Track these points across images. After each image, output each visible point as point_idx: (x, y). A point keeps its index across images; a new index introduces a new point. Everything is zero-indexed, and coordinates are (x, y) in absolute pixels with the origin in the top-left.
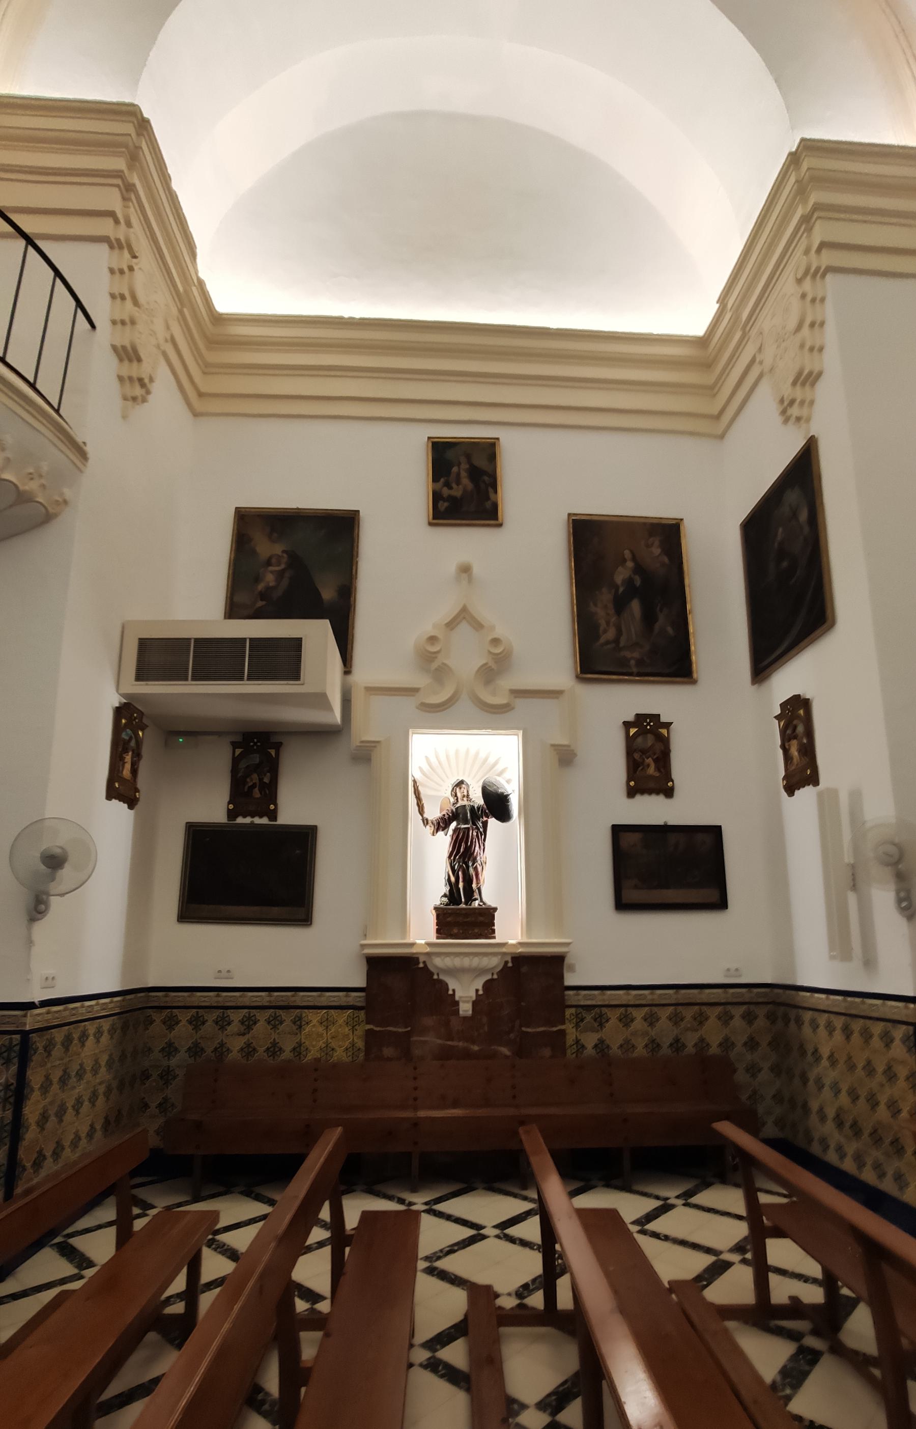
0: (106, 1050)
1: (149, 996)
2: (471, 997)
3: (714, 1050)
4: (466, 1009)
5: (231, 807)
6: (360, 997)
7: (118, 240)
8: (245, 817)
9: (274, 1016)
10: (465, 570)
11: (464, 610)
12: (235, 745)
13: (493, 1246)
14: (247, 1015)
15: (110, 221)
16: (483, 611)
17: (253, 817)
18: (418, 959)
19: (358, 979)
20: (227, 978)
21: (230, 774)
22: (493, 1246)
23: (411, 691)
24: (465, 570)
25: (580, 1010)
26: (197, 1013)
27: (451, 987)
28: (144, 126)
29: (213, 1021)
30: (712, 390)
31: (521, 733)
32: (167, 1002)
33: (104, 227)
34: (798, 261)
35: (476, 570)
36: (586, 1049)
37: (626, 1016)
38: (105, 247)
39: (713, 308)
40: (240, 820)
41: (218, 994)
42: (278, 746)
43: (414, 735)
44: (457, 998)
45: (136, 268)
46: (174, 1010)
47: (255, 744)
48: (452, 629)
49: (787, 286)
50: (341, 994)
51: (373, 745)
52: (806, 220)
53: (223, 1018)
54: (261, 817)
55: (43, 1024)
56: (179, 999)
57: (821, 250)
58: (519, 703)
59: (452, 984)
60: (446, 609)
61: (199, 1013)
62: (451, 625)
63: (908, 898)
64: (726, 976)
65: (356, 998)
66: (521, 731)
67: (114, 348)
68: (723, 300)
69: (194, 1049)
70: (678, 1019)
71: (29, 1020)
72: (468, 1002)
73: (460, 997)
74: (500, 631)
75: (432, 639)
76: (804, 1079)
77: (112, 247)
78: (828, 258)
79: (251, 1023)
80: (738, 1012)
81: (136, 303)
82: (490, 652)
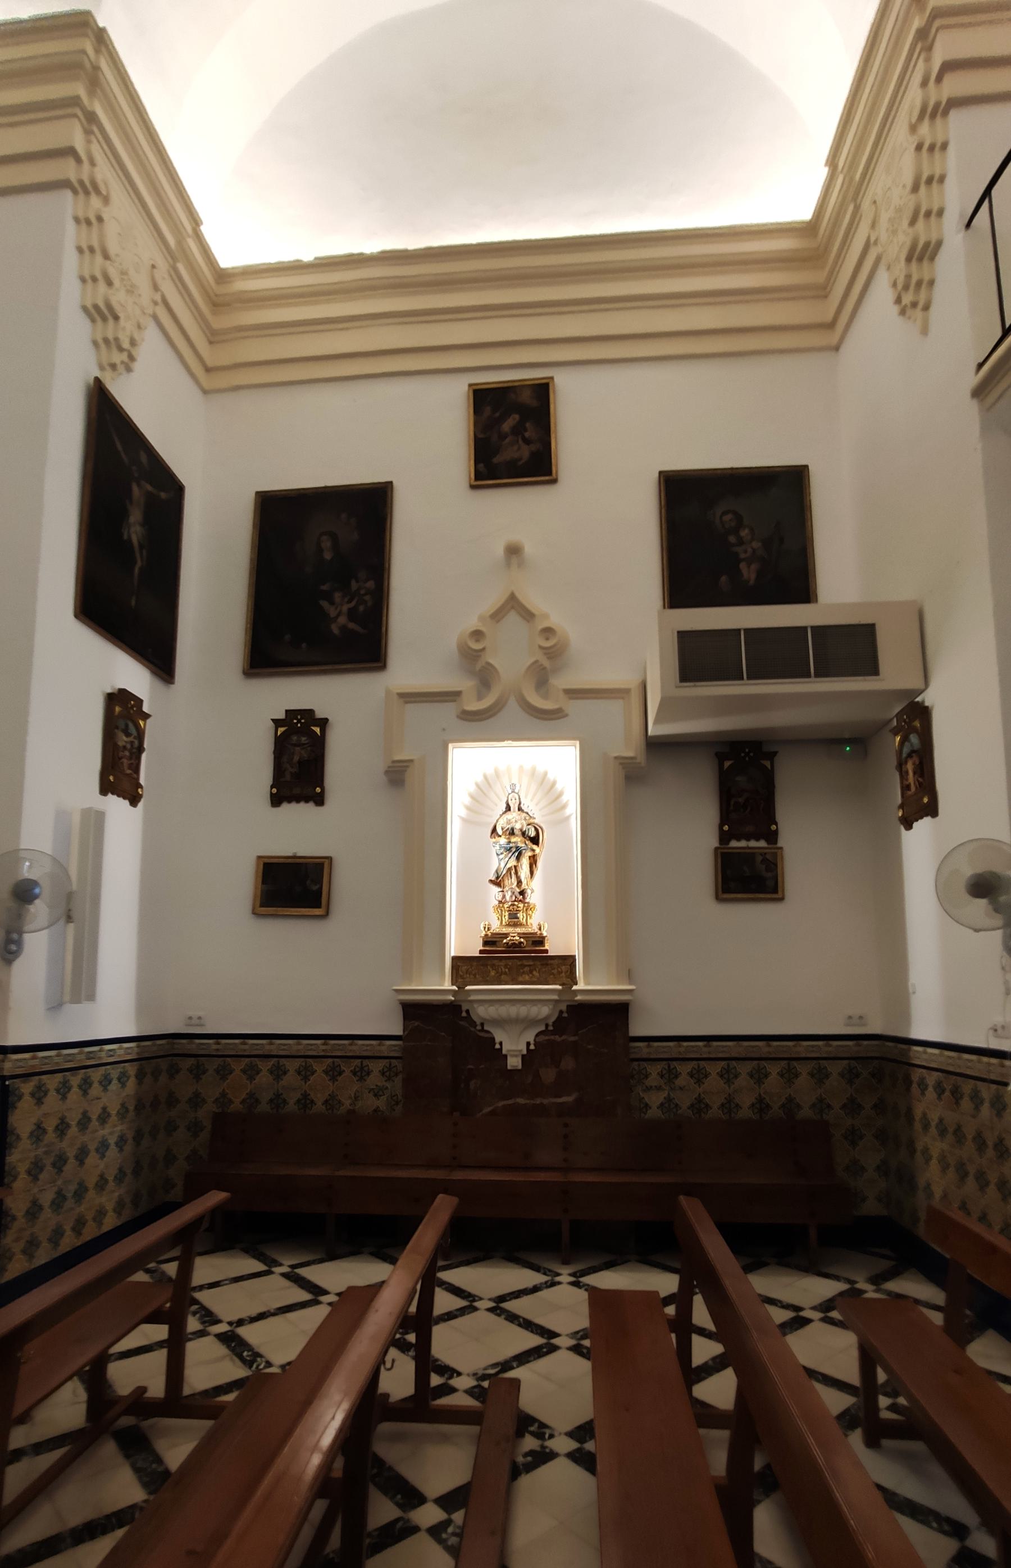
0: (92, 1100)
1: (174, 1043)
2: (520, 1051)
3: (806, 1112)
4: (514, 1062)
6: (395, 1046)
7: (81, 182)
8: (738, 840)
9: (388, 1066)
10: (513, 551)
11: (512, 597)
12: (720, 757)
13: (482, 1318)
14: (696, 1067)
15: (71, 162)
16: (534, 599)
17: (748, 839)
18: (460, 1006)
19: (395, 1027)
20: (197, 1025)
22: (482, 1318)
23: (451, 696)
24: (513, 551)
25: (853, 1063)
26: (333, 1062)
27: (497, 1040)
28: (101, 37)
29: (215, 1070)
30: (822, 291)
31: (578, 743)
32: (245, 1050)
33: (67, 170)
34: (914, 97)
35: (528, 549)
36: (288, 1104)
37: (728, 1071)
38: (68, 194)
39: (822, 173)
40: (734, 844)
41: (325, 1042)
42: (772, 756)
43: (454, 749)
44: (504, 1052)
45: (105, 216)
48: (498, 621)
49: (900, 136)
50: (671, 1044)
51: (405, 764)
52: (922, 34)
53: (362, 1068)
54: (757, 840)
55: (26, 1071)
57: (948, 113)
58: (574, 707)
59: (499, 1036)
60: (493, 600)
61: (280, 1062)
62: (497, 616)
63: (9, 941)
64: (847, 1025)
66: (578, 742)
67: (85, 309)
68: (832, 162)
69: (303, 1101)
70: (281, 1073)
71: (7, 1065)
72: (516, 1056)
73: (508, 1051)
74: (555, 620)
75: (477, 635)
76: (912, 1152)
77: (75, 192)
78: (957, 85)
79: (336, 1073)
80: (319, 1067)
81: (106, 256)
82: (540, 647)
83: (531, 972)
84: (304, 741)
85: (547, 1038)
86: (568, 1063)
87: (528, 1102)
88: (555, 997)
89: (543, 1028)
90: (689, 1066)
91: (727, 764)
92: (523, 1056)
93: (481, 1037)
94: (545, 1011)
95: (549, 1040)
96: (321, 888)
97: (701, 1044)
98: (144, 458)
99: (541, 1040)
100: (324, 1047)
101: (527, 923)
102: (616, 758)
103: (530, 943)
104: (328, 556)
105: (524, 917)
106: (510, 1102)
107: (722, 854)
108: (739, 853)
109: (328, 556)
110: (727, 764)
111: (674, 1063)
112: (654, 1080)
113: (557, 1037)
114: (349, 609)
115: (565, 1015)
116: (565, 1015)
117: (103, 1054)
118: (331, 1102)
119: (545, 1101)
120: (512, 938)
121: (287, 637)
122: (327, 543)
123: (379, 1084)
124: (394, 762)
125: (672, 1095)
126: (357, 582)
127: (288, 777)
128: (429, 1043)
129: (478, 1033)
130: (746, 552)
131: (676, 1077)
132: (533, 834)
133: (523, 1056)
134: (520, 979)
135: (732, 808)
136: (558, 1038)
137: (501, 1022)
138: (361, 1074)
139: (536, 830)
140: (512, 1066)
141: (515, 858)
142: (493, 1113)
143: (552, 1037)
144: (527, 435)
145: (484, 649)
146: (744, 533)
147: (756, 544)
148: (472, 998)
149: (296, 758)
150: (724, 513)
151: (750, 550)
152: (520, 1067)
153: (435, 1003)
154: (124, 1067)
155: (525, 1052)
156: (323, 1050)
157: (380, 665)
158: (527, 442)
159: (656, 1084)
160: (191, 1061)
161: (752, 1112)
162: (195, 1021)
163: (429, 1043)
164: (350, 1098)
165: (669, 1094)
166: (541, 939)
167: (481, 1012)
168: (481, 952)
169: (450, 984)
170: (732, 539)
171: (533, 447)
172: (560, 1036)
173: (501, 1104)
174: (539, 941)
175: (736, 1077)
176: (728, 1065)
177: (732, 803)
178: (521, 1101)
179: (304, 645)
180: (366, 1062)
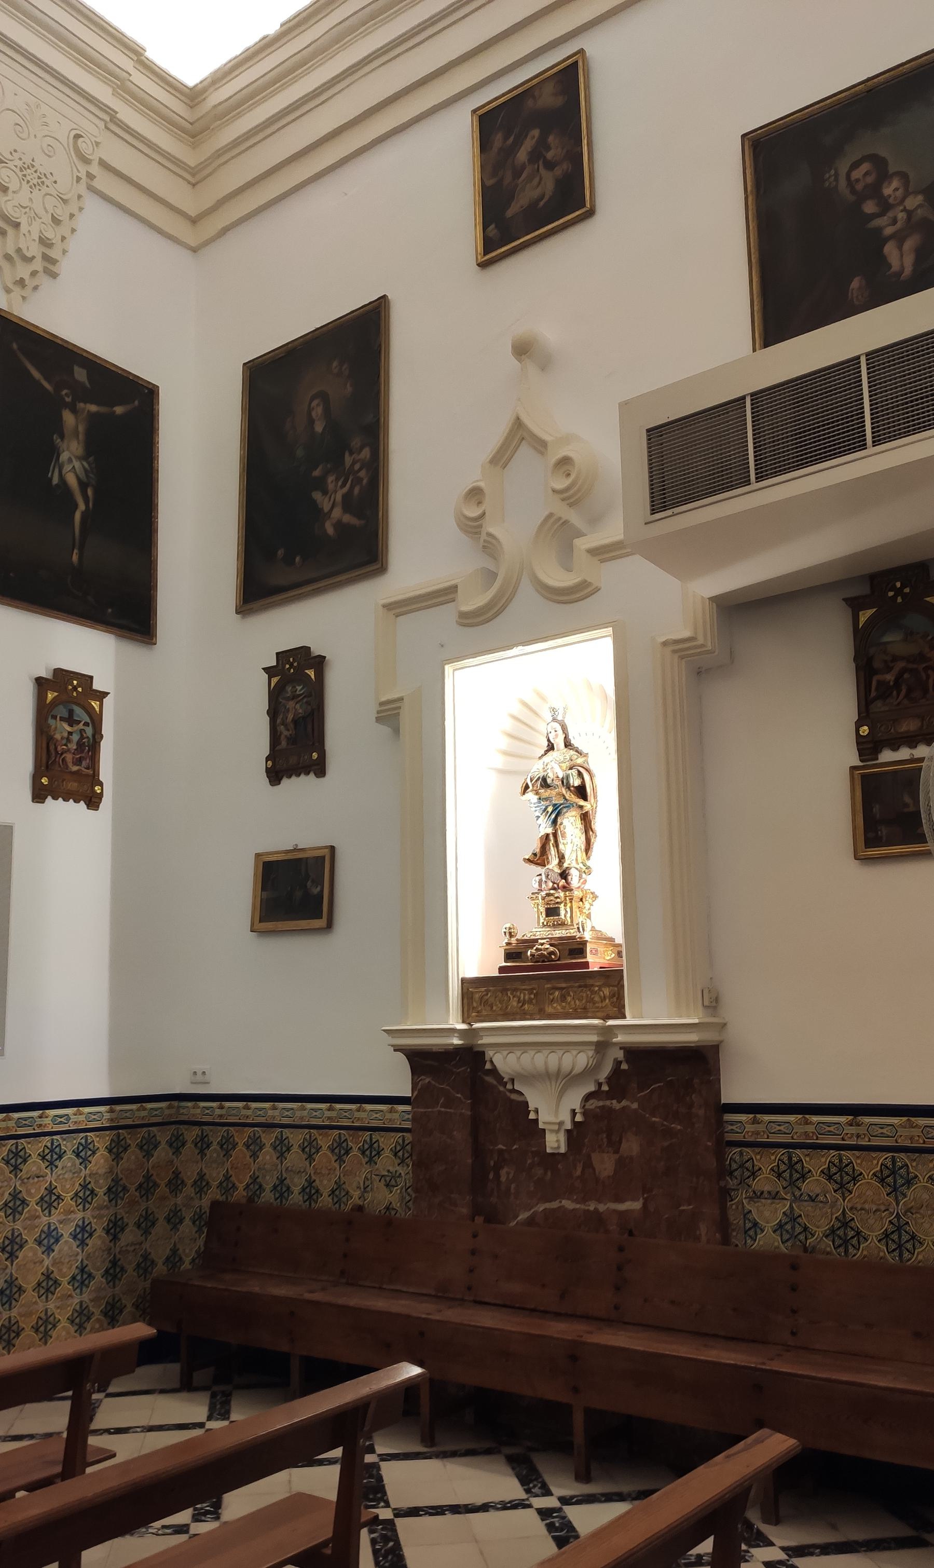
2: (561, 1124)
4: (555, 1142)
5: (865, 730)
8: (895, 748)
11: (518, 424)
12: (855, 605)
17: (913, 745)
18: (483, 1053)
21: (853, 665)
27: (531, 1107)
40: (887, 756)
44: (541, 1126)
46: (204, 1127)
47: (899, 592)
50: (792, 1118)
56: (156, 1113)
65: (401, 1115)
75: (475, 494)
80: (325, 1141)
83: (563, 998)
84: (301, 690)
85: (601, 1103)
86: (632, 1146)
87: (578, 1206)
88: (594, 1038)
89: (592, 1088)
90: (824, 1160)
91: (865, 615)
92: (568, 1132)
93: (513, 1101)
94: (582, 1060)
95: (603, 1107)
96: (322, 891)
97: (842, 1119)
98: (80, 374)
99: (593, 1107)
100: (328, 1114)
101: (572, 921)
102: (665, 644)
103: (567, 952)
104: (319, 428)
105: (566, 911)
106: (554, 1205)
107: (864, 777)
108: (895, 772)
109: (319, 428)
110: (865, 615)
111: (798, 1151)
112: (764, 1182)
113: (614, 1102)
114: (345, 497)
115: (624, 1066)
116: (624, 1066)
117: (47, 1121)
118: (338, 1191)
119: (602, 1208)
120: (540, 947)
121: (281, 553)
122: (318, 412)
123: (391, 1169)
124: (381, 704)
125: (797, 1211)
126: (351, 453)
127: (284, 743)
128: (443, 1109)
129: (508, 1094)
130: (894, 221)
131: (803, 1177)
132: (577, 782)
133: (568, 1132)
134: (549, 1010)
135: (873, 694)
136: (615, 1104)
137: (532, 1078)
138: (371, 1153)
139: (580, 774)
140: (552, 1148)
141: (550, 823)
142: (531, 1222)
143: (608, 1103)
144: (550, 155)
145: (484, 514)
146: (891, 189)
147: (912, 202)
148: (485, 1040)
149: (290, 717)
150: (855, 165)
151: (901, 216)
152: (563, 1150)
153: (435, 1049)
154: (228, 1130)
155: (569, 1126)
156: (329, 1118)
157: (379, 566)
158: (550, 166)
159: (770, 1189)
160: (196, 1131)
161: (885, 1248)
162: (199, 1077)
163: (443, 1109)
164: (358, 1188)
165: (791, 1207)
166: (581, 946)
167: (504, 1062)
168: (502, 969)
169: (460, 1021)
170: (869, 207)
171: (558, 171)
172: (619, 1102)
173: (541, 1207)
174: (578, 949)
175: (909, 1182)
176: (894, 1160)
177: (874, 684)
178: (568, 1204)
179: (298, 559)
180: (376, 1136)
